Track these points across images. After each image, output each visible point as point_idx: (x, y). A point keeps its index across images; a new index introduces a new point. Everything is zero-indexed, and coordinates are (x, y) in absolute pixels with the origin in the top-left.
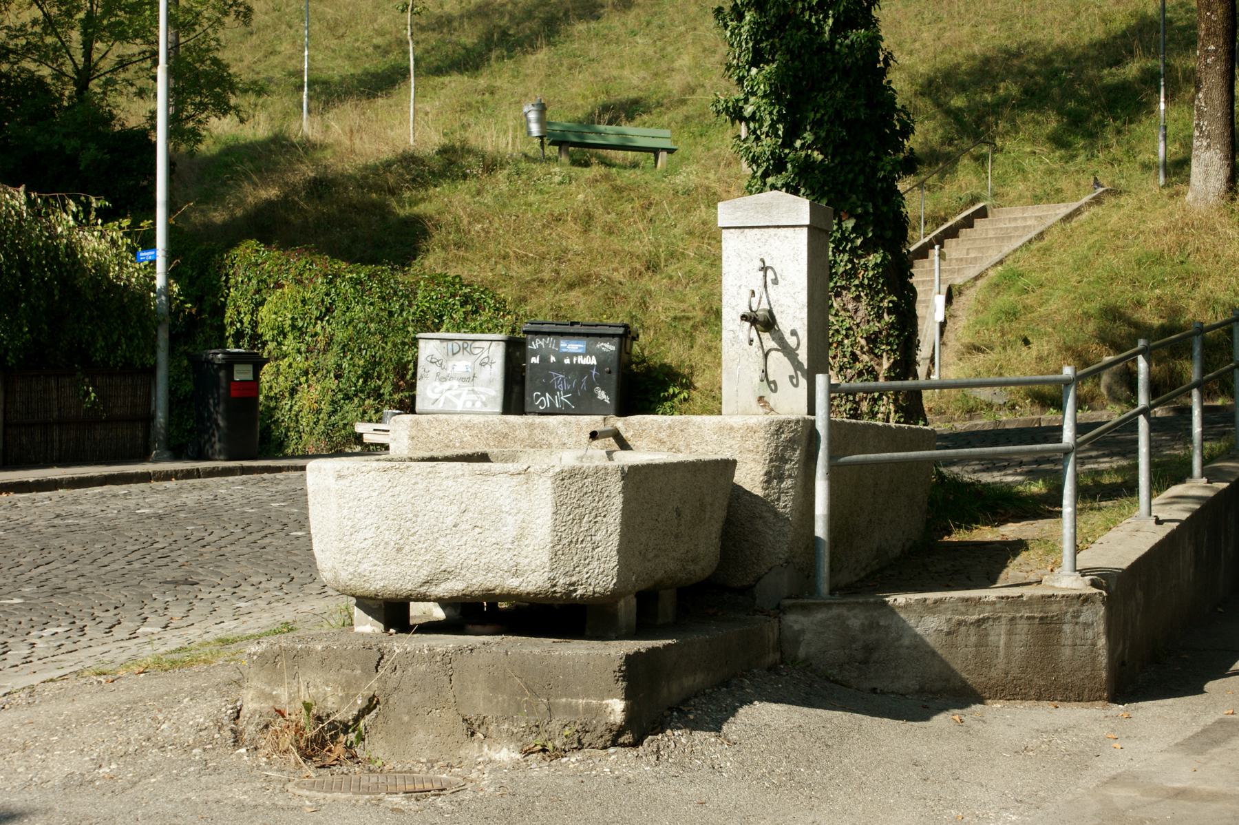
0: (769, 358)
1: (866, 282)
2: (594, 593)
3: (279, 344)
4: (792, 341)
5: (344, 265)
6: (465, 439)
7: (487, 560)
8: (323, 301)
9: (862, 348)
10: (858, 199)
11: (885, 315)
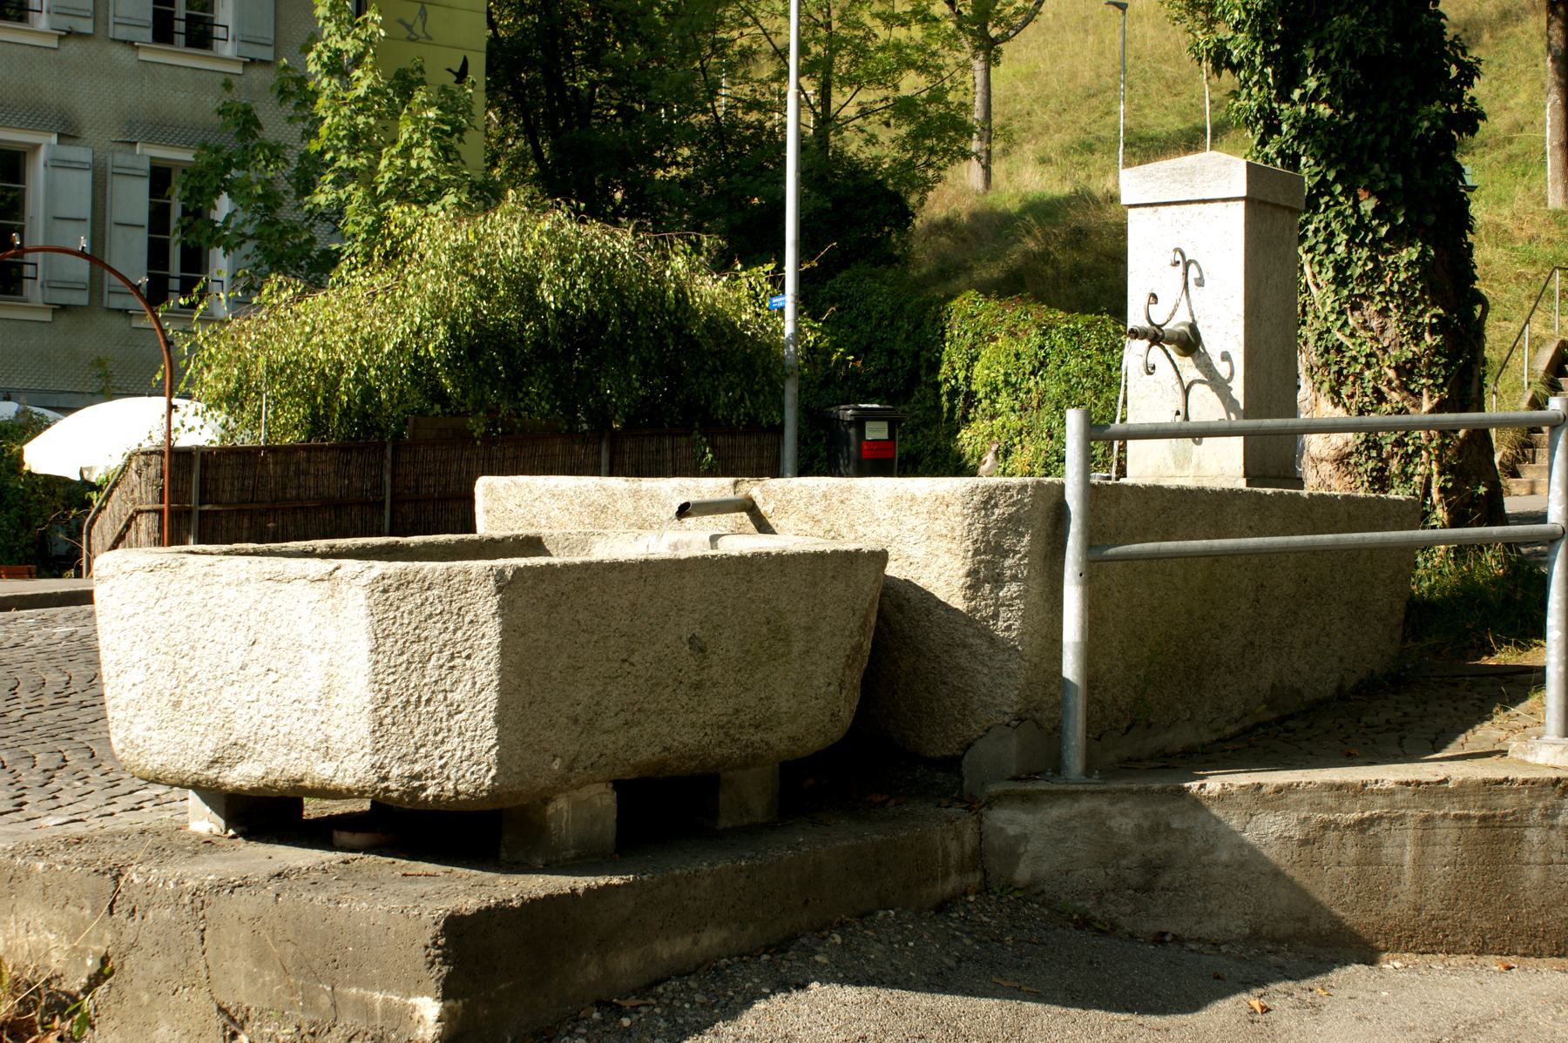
0: (1191, 393)
1: (1396, 288)
2: (457, 793)
3: (993, 402)
4: (1223, 369)
5: (1060, 314)
6: (552, 514)
7: (287, 729)
8: (1036, 354)
9: (1390, 382)
10: (1382, 169)
11: (1427, 335)
